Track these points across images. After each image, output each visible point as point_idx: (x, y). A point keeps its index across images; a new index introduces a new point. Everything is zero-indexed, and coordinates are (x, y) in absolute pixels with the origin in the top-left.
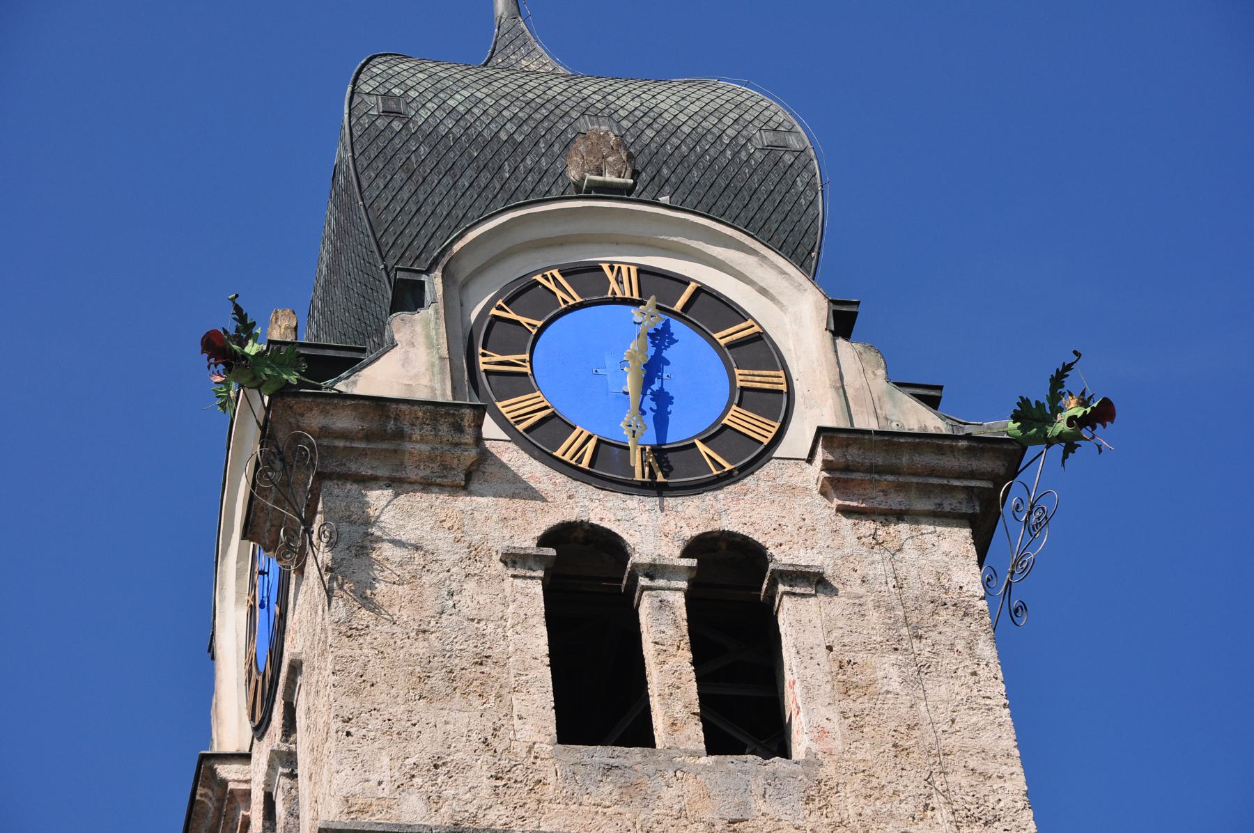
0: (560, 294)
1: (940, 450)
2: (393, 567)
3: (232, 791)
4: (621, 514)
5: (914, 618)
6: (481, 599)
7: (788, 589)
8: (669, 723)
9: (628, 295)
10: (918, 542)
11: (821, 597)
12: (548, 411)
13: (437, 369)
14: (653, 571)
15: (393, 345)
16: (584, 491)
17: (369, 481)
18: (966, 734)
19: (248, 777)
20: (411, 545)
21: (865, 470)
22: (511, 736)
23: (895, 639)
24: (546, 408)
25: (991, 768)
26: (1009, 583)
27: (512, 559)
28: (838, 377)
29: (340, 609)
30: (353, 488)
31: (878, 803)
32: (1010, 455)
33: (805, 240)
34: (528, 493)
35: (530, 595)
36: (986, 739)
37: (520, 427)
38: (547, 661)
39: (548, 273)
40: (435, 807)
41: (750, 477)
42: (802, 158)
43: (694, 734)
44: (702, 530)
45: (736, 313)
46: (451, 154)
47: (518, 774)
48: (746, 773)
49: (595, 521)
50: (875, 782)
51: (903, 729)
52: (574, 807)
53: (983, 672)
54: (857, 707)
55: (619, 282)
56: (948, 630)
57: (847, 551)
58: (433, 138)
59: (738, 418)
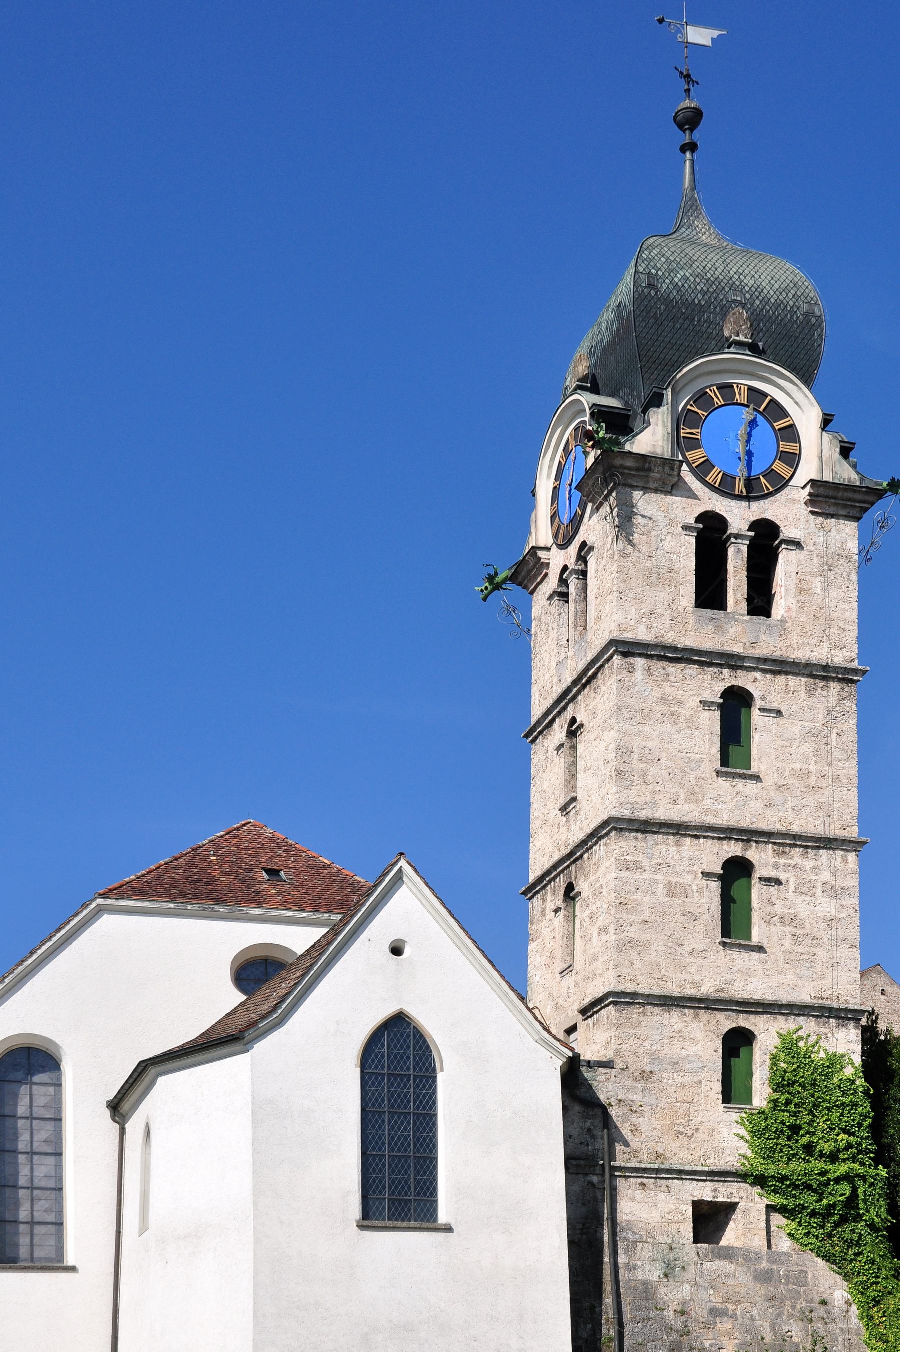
0: (716, 399)
1: (855, 491)
4: (728, 509)
14: (737, 536)
16: (715, 496)
17: (635, 487)
21: (828, 499)
27: (686, 528)
29: (621, 545)
35: (690, 543)
37: (694, 465)
43: (744, 606)
45: (782, 412)
47: (680, 619)
49: (718, 511)
55: (740, 394)
58: (667, 300)
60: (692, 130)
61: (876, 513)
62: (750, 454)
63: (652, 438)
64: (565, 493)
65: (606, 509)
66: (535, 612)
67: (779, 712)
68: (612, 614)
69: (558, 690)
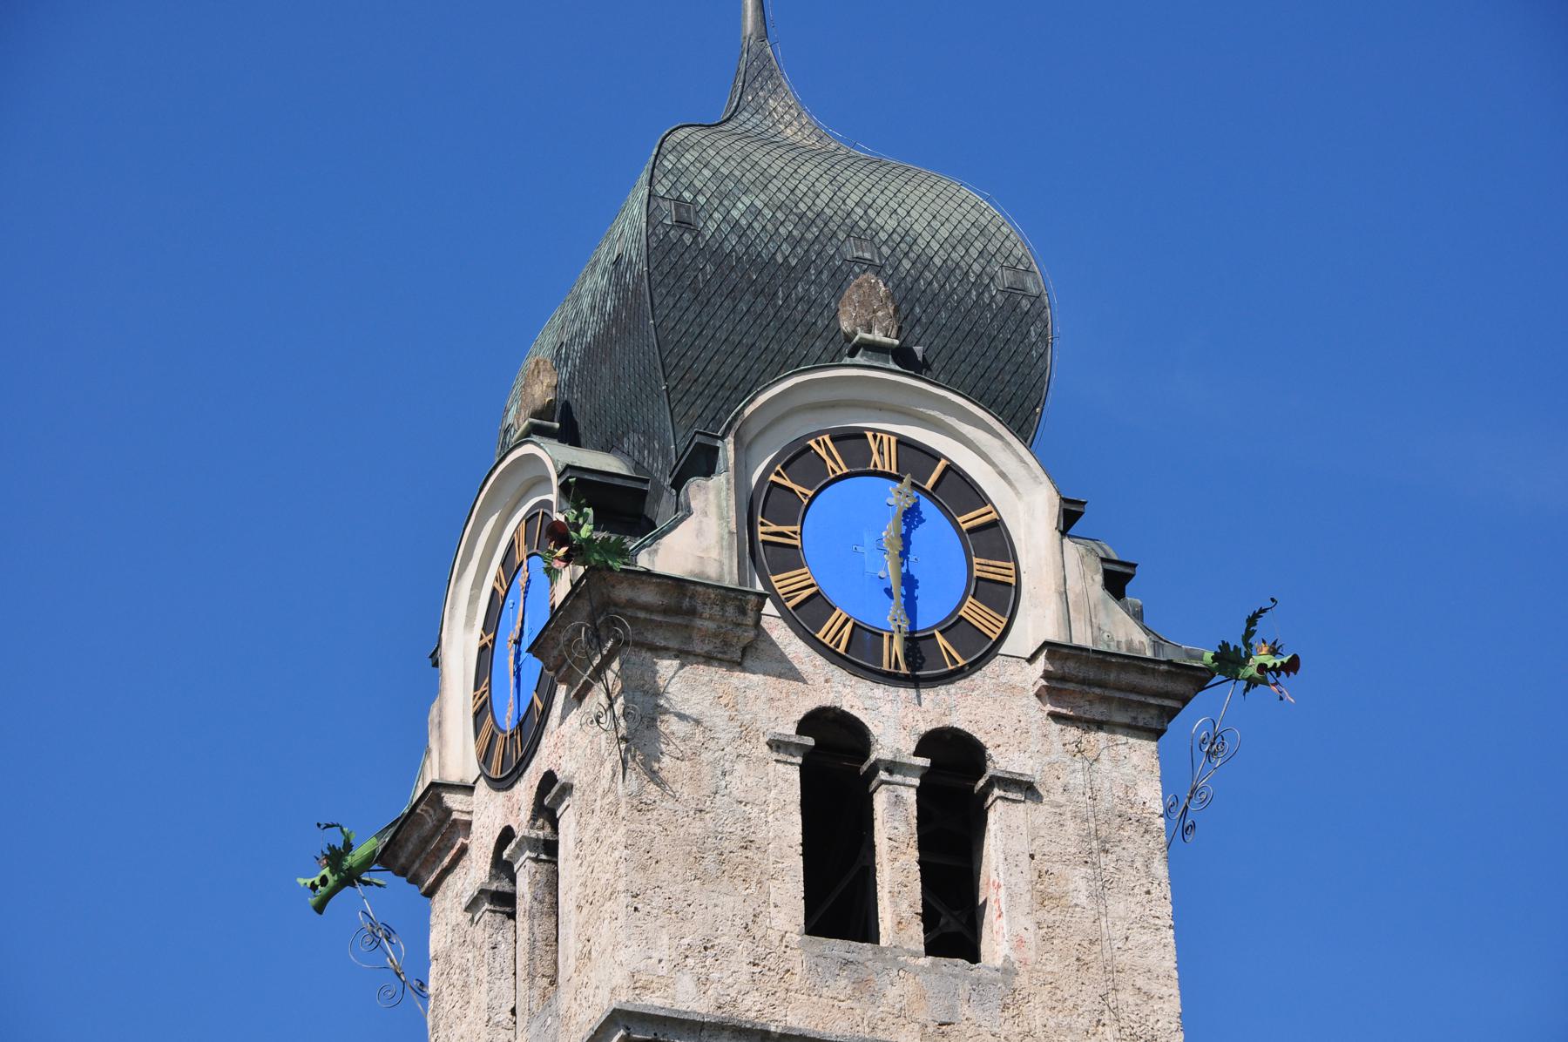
0: (830, 463)
1: (1144, 671)
4: (868, 703)
6: (748, 781)
9: (887, 469)
11: (1029, 803)
12: (813, 590)
14: (892, 767)
16: (839, 674)
17: (660, 651)
18: (1137, 952)
23: (1081, 827)
24: (812, 585)
27: (776, 745)
32: (1198, 679)
35: (788, 780)
36: (1152, 958)
38: (800, 849)
40: (703, 988)
43: (916, 932)
44: (935, 725)
45: (978, 497)
48: (956, 977)
49: (846, 708)
50: (1059, 996)
51: (1085, 944)
53: (1156, 892)
54: (1050, 918)
55: (881, 453)
57: (1054, 757)
58: (717, 255)
59: (974, 612)
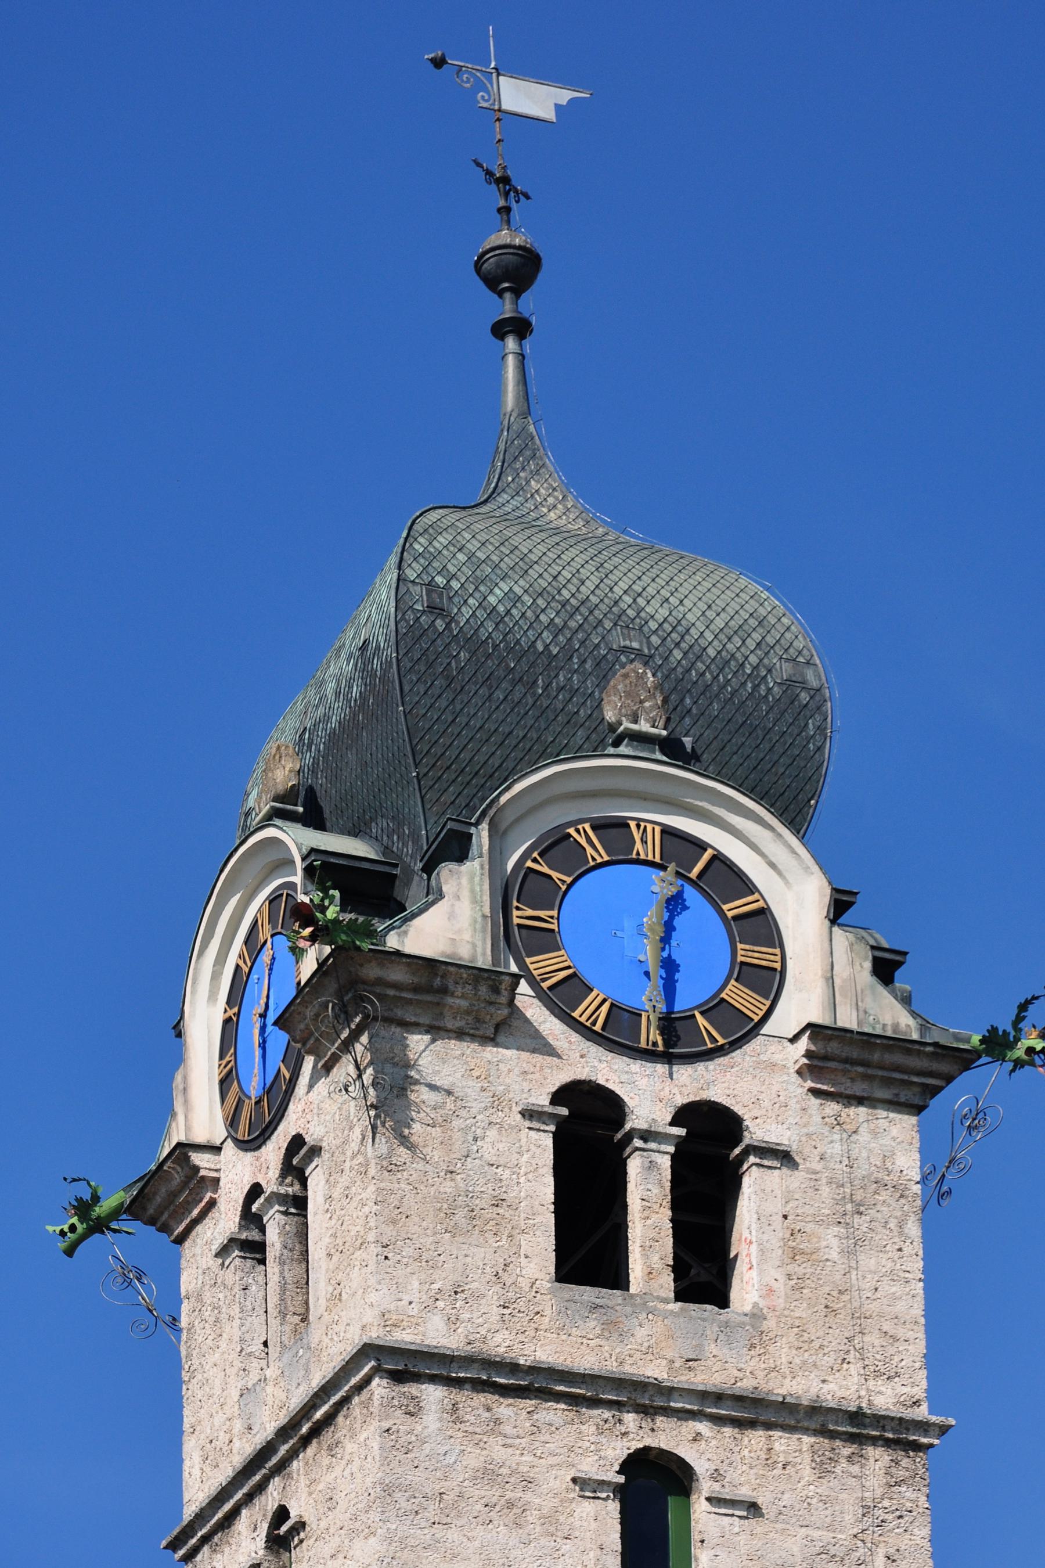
0: (589, 850)
1: (908, 1052)
2: (428, 1110)
3: (203, 1177)
4: (624, 1077)
5: (858, 1198)
6: (500, 1146)
7: (758, 1160)
8: (646, 1272)
9: (650, 857)
10: (872, 1126)
11: (785, 1170)
12: (570, 971)
13: (478, 926)
14: (647, 1136)
15: (440, 896)
16: (594, 1051)
18: (885, 1301)
19: (218, 1167)
20: (446, 1090)
21: (843, 1063)
22: (518, 1272)
24: (569, 967)
25: (901, 1332)
26: (944, 1175)
27: (530, 1114)
28: (829, 967)
30: (396, 1030)
31: (806, 1355)
33: (808, 787)
34: (546, 1049)
35: (540, 1148)
36: (900, 1307)
38: (552, 1208)
39: (580, 827)
40: (453, 1327)
41: (738, 1051)
42: (817, 698)
43: (667, 1283)
45: (743, 885)
46: (490, 663)
47: (521, 1304)
48: (704, 1320)
49: (601, 1082)
51: (835, 1293)
52: (564, 1337)
53: (907, 1249)
54: (800, 1271)
55: (644, 842)
56: (884, 1209)
57: (812, 1129)
58: (472, 641)
59: (737, 995)
60: (517, 293)
61: (958, 1097)
62: (670, 966)
63: (449, 923)
64: (250, 1031)
65: (345, 1069)
66: (188, 1281)
67: (753, 1508)
68: (357, 1302)
69: (245, 1448)
